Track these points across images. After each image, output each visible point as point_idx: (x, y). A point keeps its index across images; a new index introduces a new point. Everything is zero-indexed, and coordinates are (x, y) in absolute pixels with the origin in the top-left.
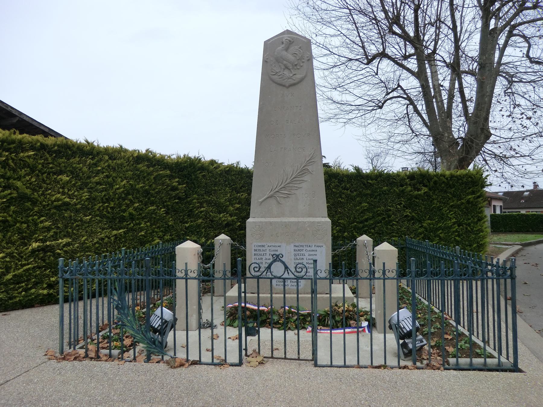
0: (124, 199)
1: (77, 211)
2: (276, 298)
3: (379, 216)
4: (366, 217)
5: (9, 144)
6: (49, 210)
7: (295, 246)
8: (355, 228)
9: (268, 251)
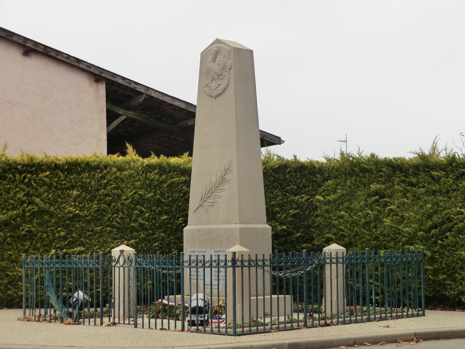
0: (133, 209)
6: (64, 221)
7: (215, 251)
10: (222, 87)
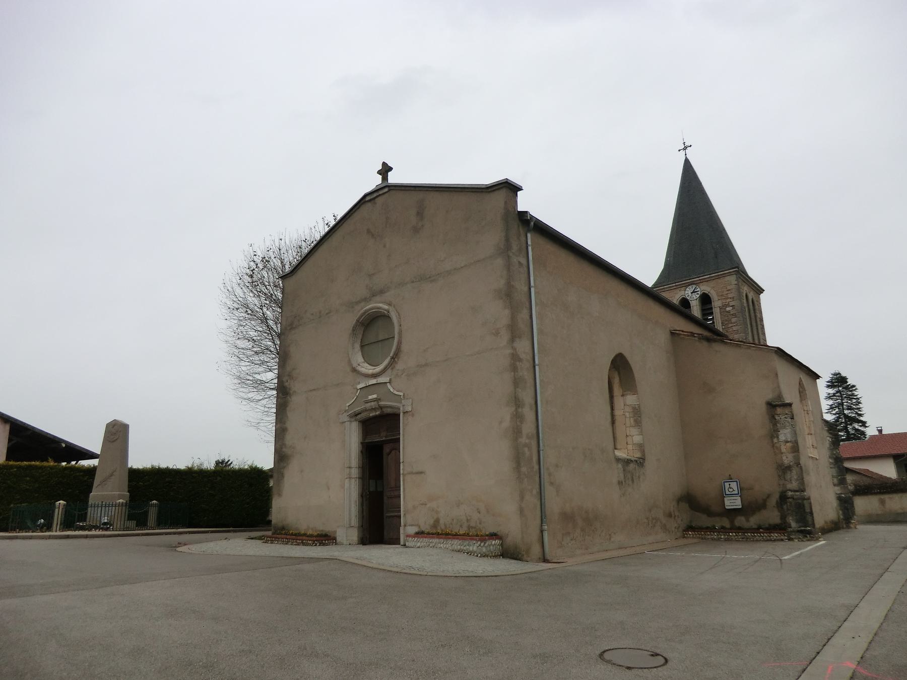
10: (115, 438)
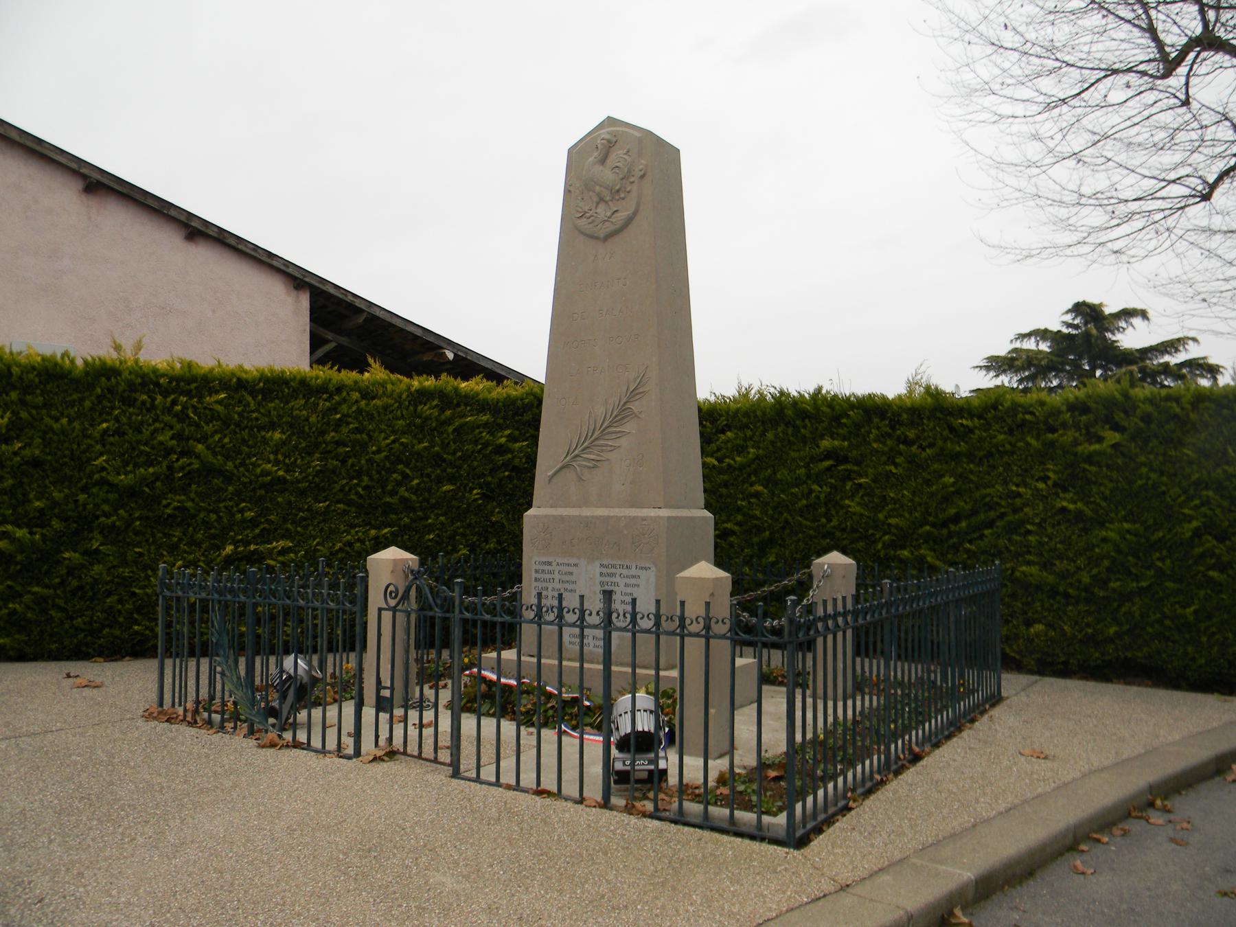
1: (302, 493)
2: (589, 669)
3: (991, 508)
4: (952, 511)
5: (189, 382)
6: (254, 490)
7: (602, 565)
8: (928, 538)
9: (556, 573)
